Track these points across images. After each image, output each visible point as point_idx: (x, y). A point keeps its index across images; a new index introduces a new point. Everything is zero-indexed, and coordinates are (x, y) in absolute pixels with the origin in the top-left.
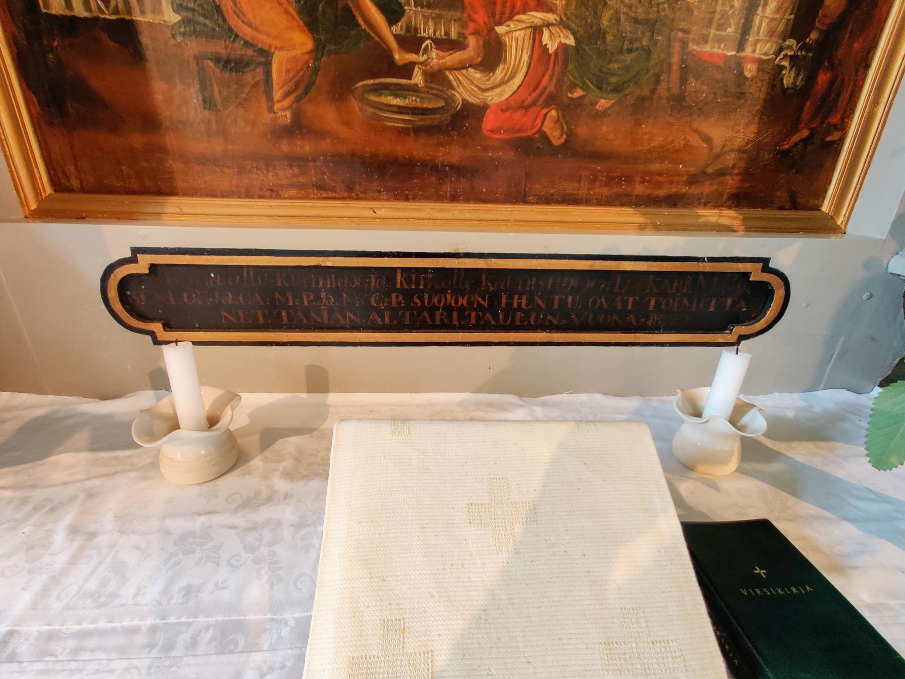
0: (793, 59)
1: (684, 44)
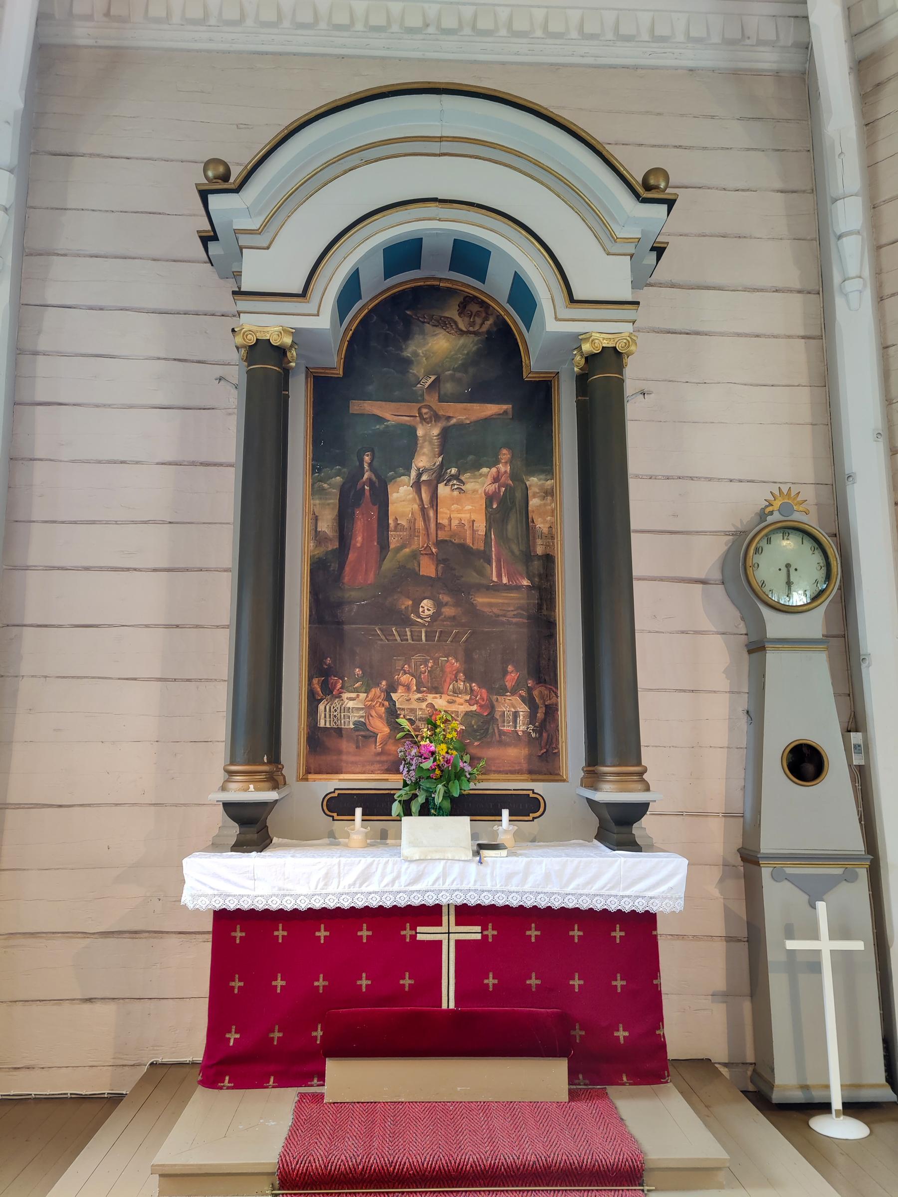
0: (532, 730)
1: (498, 728)
